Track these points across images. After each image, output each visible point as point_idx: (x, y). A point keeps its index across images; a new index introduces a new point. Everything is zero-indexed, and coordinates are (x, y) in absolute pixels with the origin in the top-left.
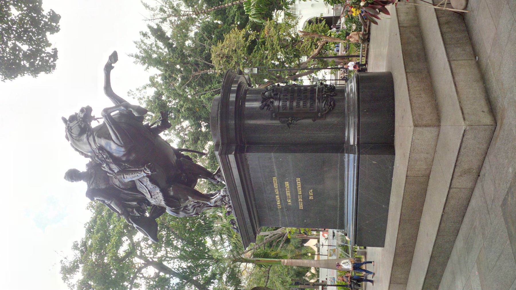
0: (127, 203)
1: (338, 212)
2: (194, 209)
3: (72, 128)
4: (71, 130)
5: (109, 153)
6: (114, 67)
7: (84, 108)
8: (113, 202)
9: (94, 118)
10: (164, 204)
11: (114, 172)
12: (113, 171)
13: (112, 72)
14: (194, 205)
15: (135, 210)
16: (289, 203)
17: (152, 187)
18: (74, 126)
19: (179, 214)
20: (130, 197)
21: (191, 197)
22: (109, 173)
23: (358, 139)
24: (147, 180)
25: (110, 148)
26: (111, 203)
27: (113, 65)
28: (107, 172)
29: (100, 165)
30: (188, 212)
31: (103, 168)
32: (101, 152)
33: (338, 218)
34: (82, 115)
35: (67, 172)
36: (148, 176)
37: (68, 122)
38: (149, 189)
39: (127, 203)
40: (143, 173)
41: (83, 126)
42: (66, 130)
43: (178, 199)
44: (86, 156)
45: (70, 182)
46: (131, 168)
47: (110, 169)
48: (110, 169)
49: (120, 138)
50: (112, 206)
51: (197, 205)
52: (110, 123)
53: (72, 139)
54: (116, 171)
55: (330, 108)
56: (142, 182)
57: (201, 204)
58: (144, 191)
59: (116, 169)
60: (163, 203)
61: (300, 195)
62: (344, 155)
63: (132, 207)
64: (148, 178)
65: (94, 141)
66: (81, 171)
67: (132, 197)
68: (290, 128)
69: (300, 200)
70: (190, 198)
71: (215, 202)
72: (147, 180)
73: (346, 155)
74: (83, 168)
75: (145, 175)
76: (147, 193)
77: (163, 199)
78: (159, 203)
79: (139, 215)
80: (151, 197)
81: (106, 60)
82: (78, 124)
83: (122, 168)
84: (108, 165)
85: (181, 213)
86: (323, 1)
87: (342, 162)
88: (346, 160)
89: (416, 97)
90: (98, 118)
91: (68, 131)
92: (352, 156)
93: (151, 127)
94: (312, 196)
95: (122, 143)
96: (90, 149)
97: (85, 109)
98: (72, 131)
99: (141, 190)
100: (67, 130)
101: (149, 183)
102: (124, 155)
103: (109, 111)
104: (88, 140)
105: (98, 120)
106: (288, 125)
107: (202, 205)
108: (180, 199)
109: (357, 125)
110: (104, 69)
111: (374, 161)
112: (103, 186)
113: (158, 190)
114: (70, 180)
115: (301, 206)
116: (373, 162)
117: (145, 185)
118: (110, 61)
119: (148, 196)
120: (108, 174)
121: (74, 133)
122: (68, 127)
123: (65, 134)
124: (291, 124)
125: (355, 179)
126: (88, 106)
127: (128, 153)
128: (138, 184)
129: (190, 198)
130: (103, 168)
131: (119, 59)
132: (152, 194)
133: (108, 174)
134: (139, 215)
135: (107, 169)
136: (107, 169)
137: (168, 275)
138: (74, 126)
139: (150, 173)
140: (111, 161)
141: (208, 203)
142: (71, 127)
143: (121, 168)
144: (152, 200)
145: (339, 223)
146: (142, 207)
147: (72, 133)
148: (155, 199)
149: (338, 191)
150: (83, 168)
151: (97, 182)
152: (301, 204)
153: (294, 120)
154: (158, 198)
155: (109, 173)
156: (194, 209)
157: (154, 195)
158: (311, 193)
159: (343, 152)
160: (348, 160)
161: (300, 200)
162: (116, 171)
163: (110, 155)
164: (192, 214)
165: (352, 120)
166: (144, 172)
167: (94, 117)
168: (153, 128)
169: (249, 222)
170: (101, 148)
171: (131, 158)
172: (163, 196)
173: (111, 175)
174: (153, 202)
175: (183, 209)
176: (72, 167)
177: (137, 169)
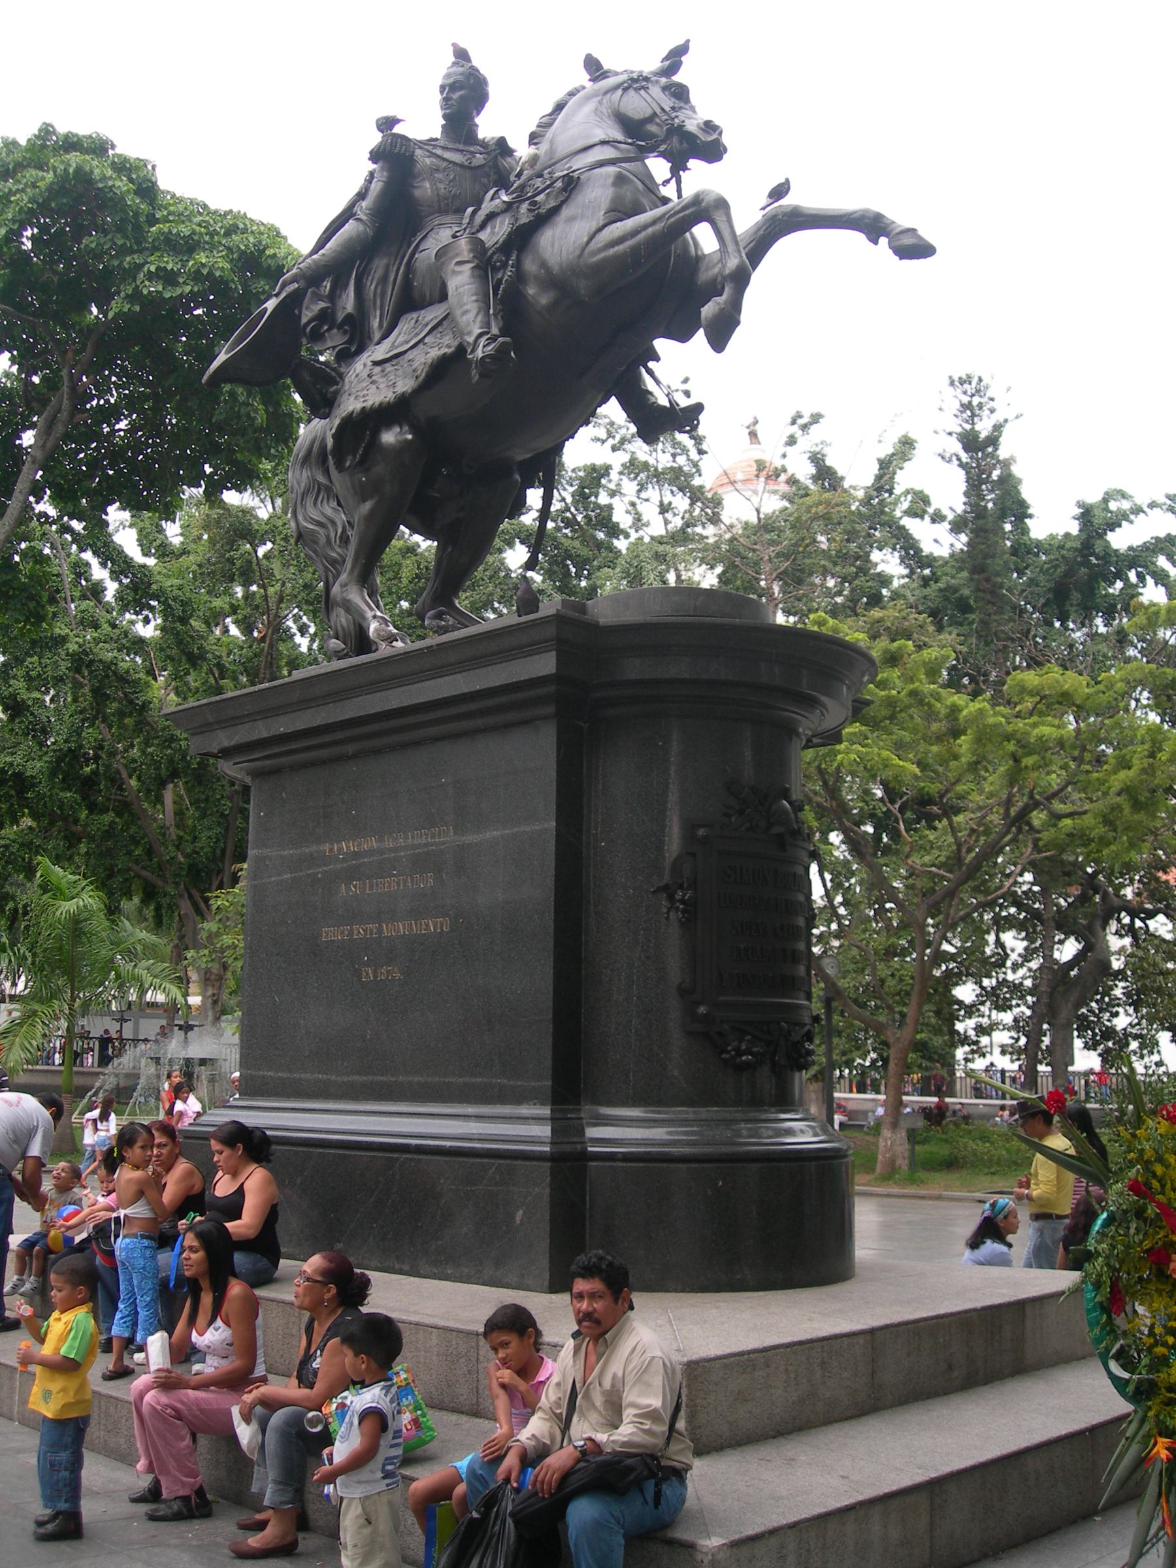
0: (352, 282)
1: (308, 1076)
2: (319, 524)
3: (642, 92)
4: (637, 90)
5: (555, 211)
6: (876, 243)
7: (720, 134)
8: (361, 228)
9: (678, 167)
10: (351, 409)
11: (478, 231)
12: (483, 226)
13: (857, 238)
14: (333, 523)
15: (322, 305)
16: (348, 889)
17: (415, 365)
18: (649, 100)
19: (302, 465)
20: (373, 287)
21: (372, 512)
22: (474, 213)
23: (611, 1157)
24: (448, 346)
25: (572, 219)
26: (359, 220)
27: (883, 241)
28: (478, 204)
29: (503, 183)
30: (309, 502)
31: (492, 192)
32: (559, 184)
33: (285, 1075)
34: (691, 126)
35: (478, 71)
36: (461, 350)
37: (664, 80)
38: (409, 355)
39: (352, 282)
40: (477, 331)
41: (653, 128)
42: (632, 72)
43: (363, 464)
44: (534, 139)
45: (439, 81)
46: (495, 294)
47: (491, 216)
48: (491, 216)
49: (612, 251)
50: (346, 226)
51: (332, 535)
52: (672, 220)
53: (603, 91)
54: (483, 236)
55: (729, 1052)
56: (440, 329)
57: (339, 550)
58: (401, 339)
59: (496, 234)
60: (350, 405)
61: (380, 931)
62: (542, 1104)
63: (333, 297)
64: (452, 349)
65: (601, 164)
66: (477, 120)
67: (371, 295)
68: (654, 892)
69: (359, 931)
70: (367, 506)
71: (348, 606)
72: (448, 346)
73: (546, 1111)
74: (487, 126)
75: (470, 339)
76: (393, 347)
77: (369, 404)
78: (354, 390)
79: (304, 320)
80: (376, 363)
81: (900, 216)
82: (658, 111)
83: (495, 257)
84: (508, 207)
85: (306, 474)
86: (1172, 492)
87: (519, 1098)
88: (524, 1110)
89: (787, 1370)
90: (679, 183)
91: (632, 79)
92: (544, 1131)
93: (643, 370)
94: (375, 977)
95: (595, 259)
96: (562, 150)
97: (715, 136)
98: (631, 92)
99: (406, 326)
100: (635, 76)
101: (435, 353)
102: (544, 265)
103: (720, 218)
104: (603, 143)
105: (673, 181)
106: (665, 888)
107: (334, 555)
108: (367, 470)
109: (667, 1153)
110: (867, 211)
111: (524, 1213)
112: (425, 190)
113: (405, 385)
114: (451, 80)
115: (331, 934)
116: (520, 1212)
117: (426, 340)
118: (898, 230)
119: (380, 352)
120: (470, 210)
121: (625, 98)
122: (647, 79)
123: (619, 70)
124: (671, 898)
125: (448, 1144)
126: (725, 150)
127: (553, 281)
128: (432, 314)
129: (367, 506)
130: (492, 192)
131: (904, 261)
132: (388, 367)
133: (470, 210)
134: (304, 320)
135: (487, 207)
136: (487, 207)
137: (32, 441)
138: (649, 100)
139: (479, 353)
140: (524, 220)
141: (344, 577)
142: (645, 88)
143: (494, 253)
144: (365, 365)
145: (263, 1077)
146: (335, 331)
147: (625, 90)
148: (370, 376)
149: (393, 1079)
150: (487, 126)
151: (437, 170)
152: (342, 933)
153: (684, 912)
154: (374, 387)
155: (474, 213)
156: (319, 524)
157: (384, 374)
158: (388, 972)
159: (554, 1103)
160: (527, 1118)
161: (359, 931)
162: (483, 236)
163: (543, 220)
164: (300, 518)
165: (686, 1133)
166: (480, 335)
167: (685, 169)
168: (639, 378)
169: (273, 732)
170: (571, 184)
171: (531, 291)
172: (380, 404)
173: (466, 221)
174: (361, 365)
175: (319, 484)
176: (494, 90)
177: (491, 311)
